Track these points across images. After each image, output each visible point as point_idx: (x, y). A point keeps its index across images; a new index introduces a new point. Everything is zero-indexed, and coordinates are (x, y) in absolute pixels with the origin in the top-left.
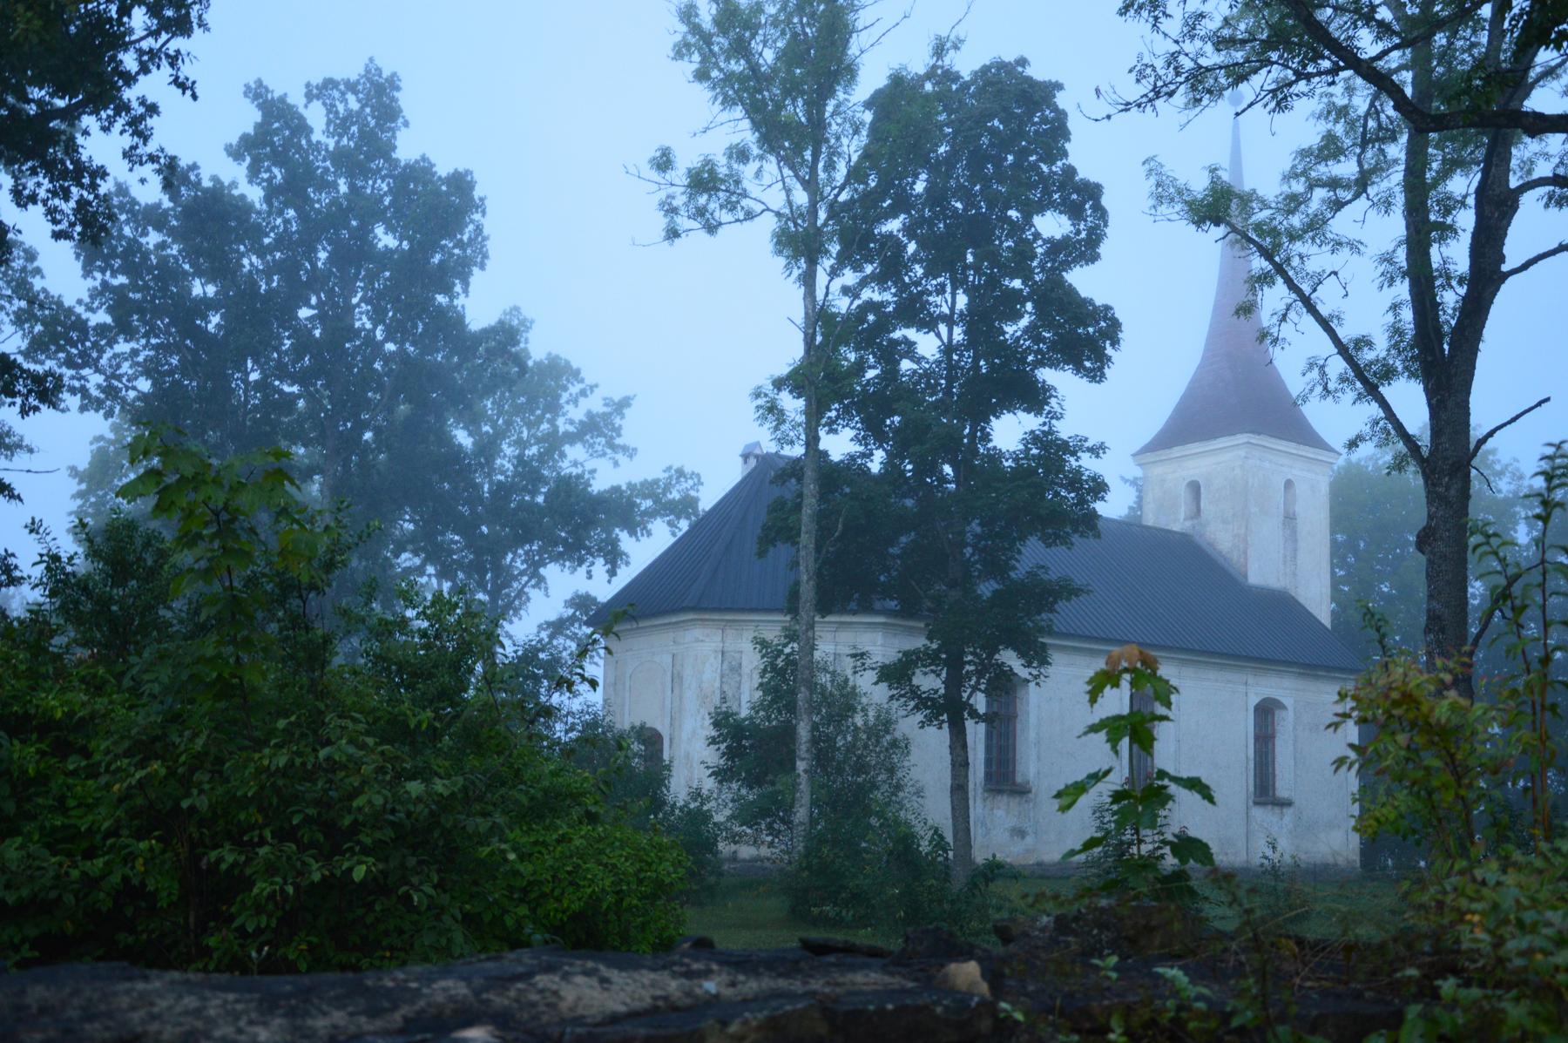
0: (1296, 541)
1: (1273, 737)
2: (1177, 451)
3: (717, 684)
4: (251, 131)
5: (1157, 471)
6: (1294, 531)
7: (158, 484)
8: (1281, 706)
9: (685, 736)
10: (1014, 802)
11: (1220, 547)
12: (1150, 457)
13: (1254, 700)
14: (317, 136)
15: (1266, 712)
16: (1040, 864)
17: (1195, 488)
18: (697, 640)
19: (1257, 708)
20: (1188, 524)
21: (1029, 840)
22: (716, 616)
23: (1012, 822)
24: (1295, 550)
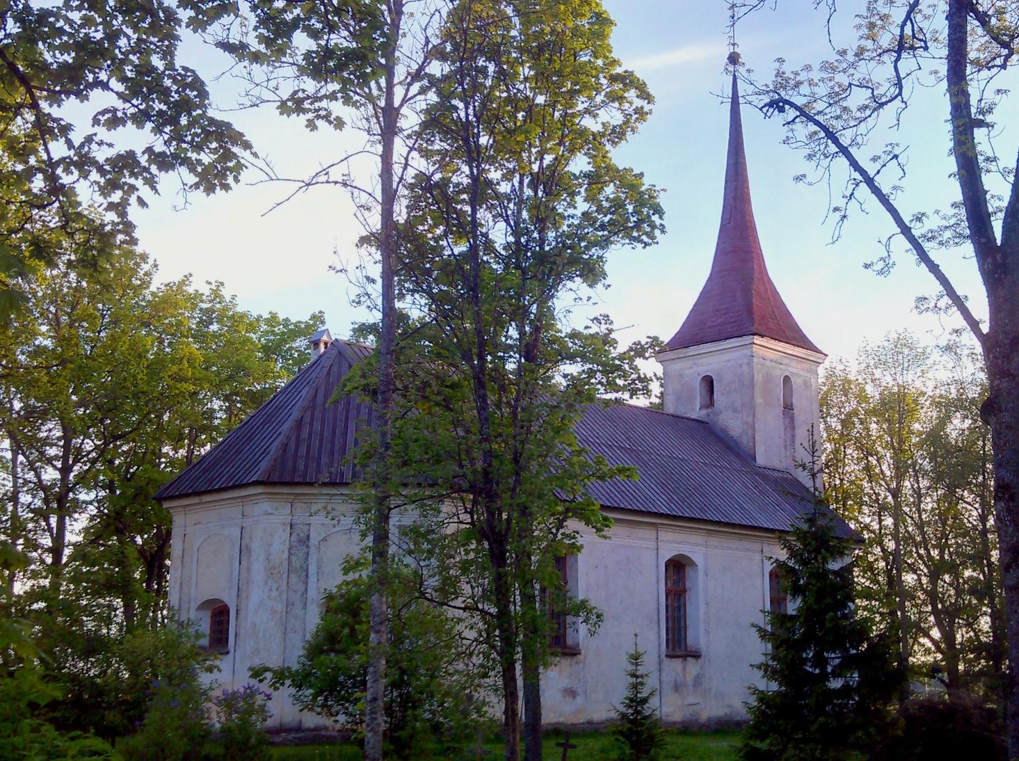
0: (793, 428)
1: (685, 591)
2: (692, 351)
3: (286, 555)
4: (225, 16)
5: (676, 366)
6: (792, 419)
7: (652, 380)
8: (693, 564)
9: (252, 606)
10: (565, 663)
11: (732, 433)
12: (670, 355)
13: (666, 555)
14: (982, 56)
15: (678, 567)
16: (590, 723)
17: (709, 382)
18: (267, 513)
19: (668, 564)
20: (704, 412)
21: (579, 699)
22: (285, 490)
23: (564, 682)
24: (793, 436)
